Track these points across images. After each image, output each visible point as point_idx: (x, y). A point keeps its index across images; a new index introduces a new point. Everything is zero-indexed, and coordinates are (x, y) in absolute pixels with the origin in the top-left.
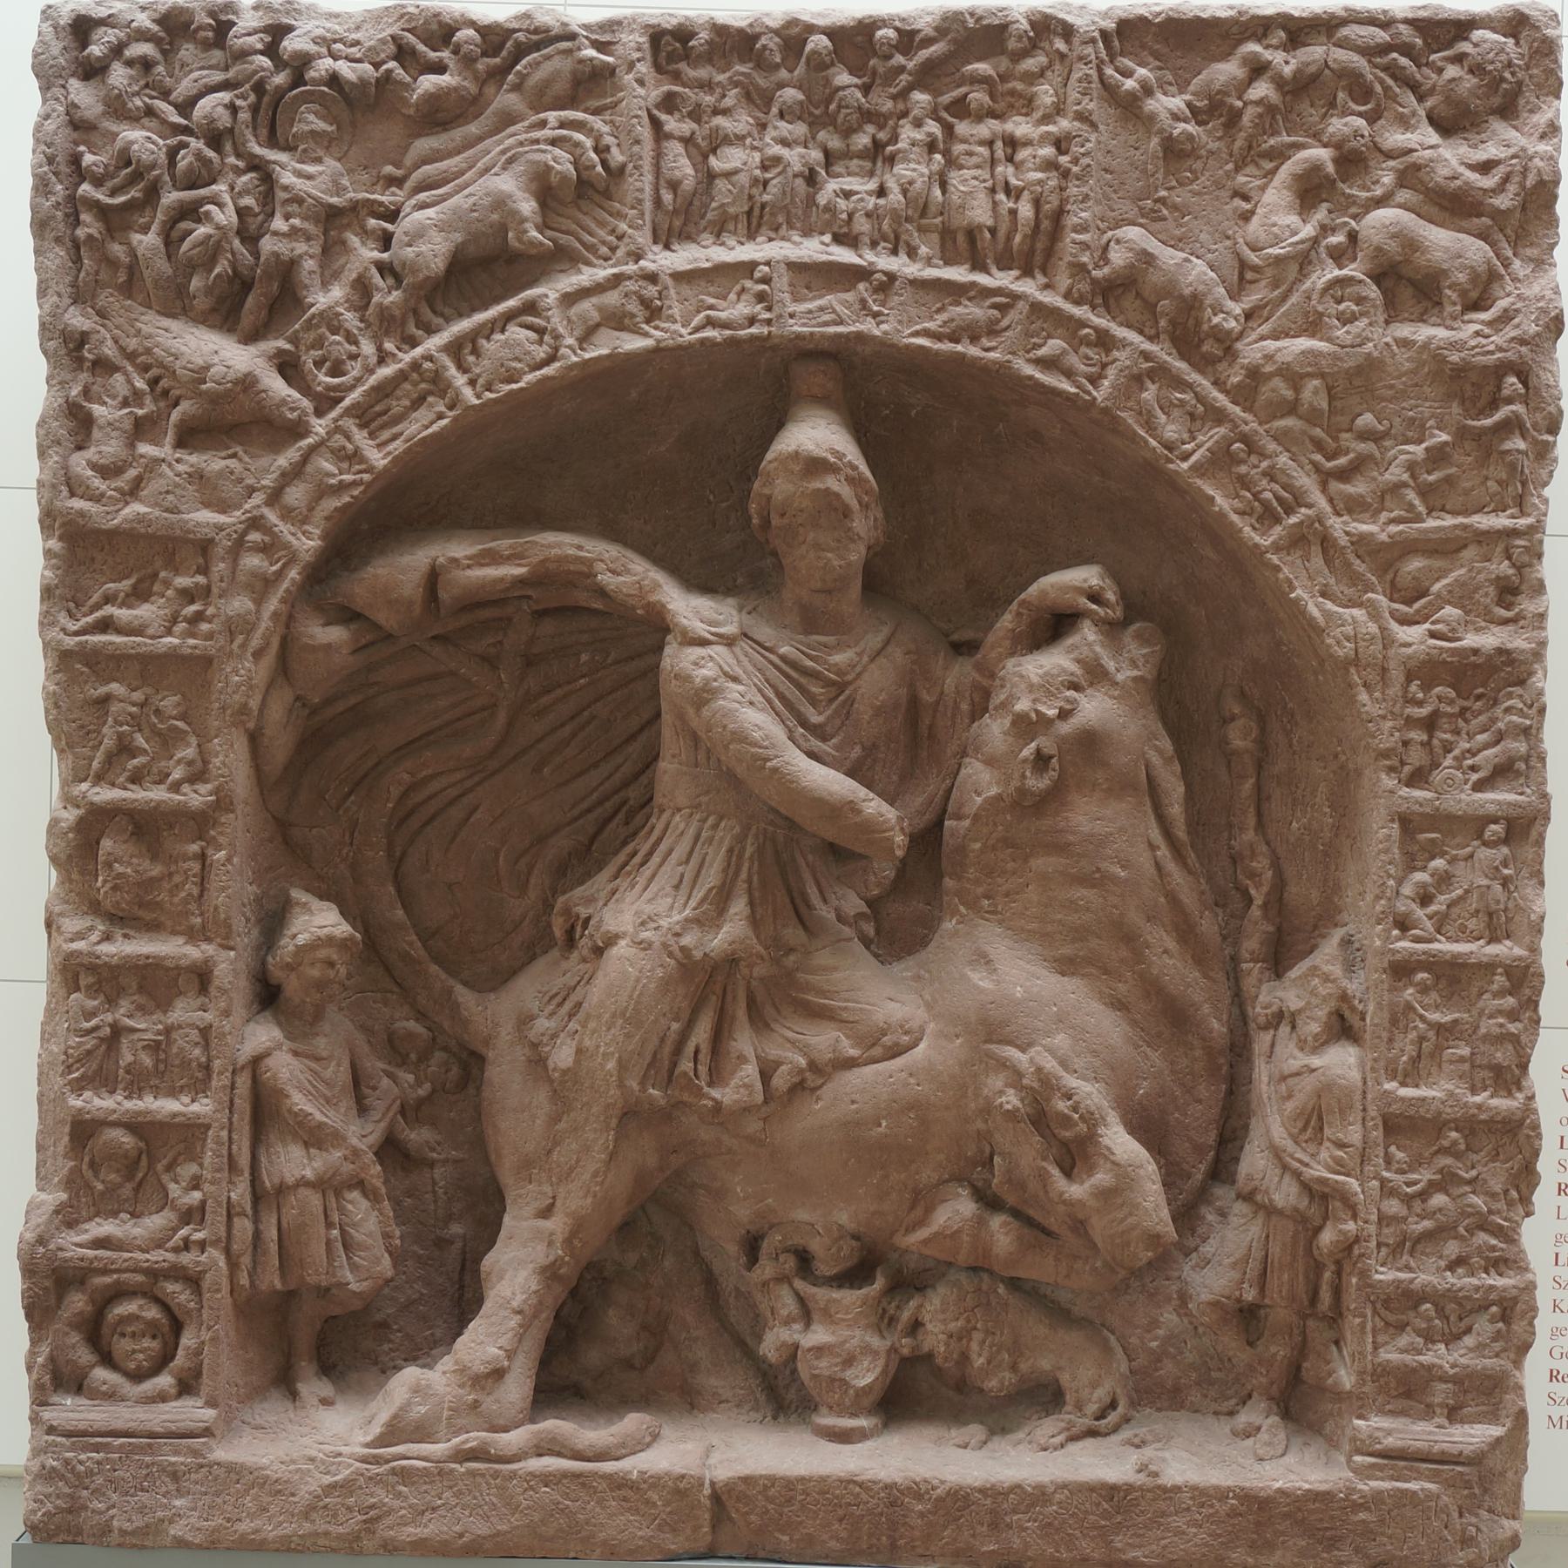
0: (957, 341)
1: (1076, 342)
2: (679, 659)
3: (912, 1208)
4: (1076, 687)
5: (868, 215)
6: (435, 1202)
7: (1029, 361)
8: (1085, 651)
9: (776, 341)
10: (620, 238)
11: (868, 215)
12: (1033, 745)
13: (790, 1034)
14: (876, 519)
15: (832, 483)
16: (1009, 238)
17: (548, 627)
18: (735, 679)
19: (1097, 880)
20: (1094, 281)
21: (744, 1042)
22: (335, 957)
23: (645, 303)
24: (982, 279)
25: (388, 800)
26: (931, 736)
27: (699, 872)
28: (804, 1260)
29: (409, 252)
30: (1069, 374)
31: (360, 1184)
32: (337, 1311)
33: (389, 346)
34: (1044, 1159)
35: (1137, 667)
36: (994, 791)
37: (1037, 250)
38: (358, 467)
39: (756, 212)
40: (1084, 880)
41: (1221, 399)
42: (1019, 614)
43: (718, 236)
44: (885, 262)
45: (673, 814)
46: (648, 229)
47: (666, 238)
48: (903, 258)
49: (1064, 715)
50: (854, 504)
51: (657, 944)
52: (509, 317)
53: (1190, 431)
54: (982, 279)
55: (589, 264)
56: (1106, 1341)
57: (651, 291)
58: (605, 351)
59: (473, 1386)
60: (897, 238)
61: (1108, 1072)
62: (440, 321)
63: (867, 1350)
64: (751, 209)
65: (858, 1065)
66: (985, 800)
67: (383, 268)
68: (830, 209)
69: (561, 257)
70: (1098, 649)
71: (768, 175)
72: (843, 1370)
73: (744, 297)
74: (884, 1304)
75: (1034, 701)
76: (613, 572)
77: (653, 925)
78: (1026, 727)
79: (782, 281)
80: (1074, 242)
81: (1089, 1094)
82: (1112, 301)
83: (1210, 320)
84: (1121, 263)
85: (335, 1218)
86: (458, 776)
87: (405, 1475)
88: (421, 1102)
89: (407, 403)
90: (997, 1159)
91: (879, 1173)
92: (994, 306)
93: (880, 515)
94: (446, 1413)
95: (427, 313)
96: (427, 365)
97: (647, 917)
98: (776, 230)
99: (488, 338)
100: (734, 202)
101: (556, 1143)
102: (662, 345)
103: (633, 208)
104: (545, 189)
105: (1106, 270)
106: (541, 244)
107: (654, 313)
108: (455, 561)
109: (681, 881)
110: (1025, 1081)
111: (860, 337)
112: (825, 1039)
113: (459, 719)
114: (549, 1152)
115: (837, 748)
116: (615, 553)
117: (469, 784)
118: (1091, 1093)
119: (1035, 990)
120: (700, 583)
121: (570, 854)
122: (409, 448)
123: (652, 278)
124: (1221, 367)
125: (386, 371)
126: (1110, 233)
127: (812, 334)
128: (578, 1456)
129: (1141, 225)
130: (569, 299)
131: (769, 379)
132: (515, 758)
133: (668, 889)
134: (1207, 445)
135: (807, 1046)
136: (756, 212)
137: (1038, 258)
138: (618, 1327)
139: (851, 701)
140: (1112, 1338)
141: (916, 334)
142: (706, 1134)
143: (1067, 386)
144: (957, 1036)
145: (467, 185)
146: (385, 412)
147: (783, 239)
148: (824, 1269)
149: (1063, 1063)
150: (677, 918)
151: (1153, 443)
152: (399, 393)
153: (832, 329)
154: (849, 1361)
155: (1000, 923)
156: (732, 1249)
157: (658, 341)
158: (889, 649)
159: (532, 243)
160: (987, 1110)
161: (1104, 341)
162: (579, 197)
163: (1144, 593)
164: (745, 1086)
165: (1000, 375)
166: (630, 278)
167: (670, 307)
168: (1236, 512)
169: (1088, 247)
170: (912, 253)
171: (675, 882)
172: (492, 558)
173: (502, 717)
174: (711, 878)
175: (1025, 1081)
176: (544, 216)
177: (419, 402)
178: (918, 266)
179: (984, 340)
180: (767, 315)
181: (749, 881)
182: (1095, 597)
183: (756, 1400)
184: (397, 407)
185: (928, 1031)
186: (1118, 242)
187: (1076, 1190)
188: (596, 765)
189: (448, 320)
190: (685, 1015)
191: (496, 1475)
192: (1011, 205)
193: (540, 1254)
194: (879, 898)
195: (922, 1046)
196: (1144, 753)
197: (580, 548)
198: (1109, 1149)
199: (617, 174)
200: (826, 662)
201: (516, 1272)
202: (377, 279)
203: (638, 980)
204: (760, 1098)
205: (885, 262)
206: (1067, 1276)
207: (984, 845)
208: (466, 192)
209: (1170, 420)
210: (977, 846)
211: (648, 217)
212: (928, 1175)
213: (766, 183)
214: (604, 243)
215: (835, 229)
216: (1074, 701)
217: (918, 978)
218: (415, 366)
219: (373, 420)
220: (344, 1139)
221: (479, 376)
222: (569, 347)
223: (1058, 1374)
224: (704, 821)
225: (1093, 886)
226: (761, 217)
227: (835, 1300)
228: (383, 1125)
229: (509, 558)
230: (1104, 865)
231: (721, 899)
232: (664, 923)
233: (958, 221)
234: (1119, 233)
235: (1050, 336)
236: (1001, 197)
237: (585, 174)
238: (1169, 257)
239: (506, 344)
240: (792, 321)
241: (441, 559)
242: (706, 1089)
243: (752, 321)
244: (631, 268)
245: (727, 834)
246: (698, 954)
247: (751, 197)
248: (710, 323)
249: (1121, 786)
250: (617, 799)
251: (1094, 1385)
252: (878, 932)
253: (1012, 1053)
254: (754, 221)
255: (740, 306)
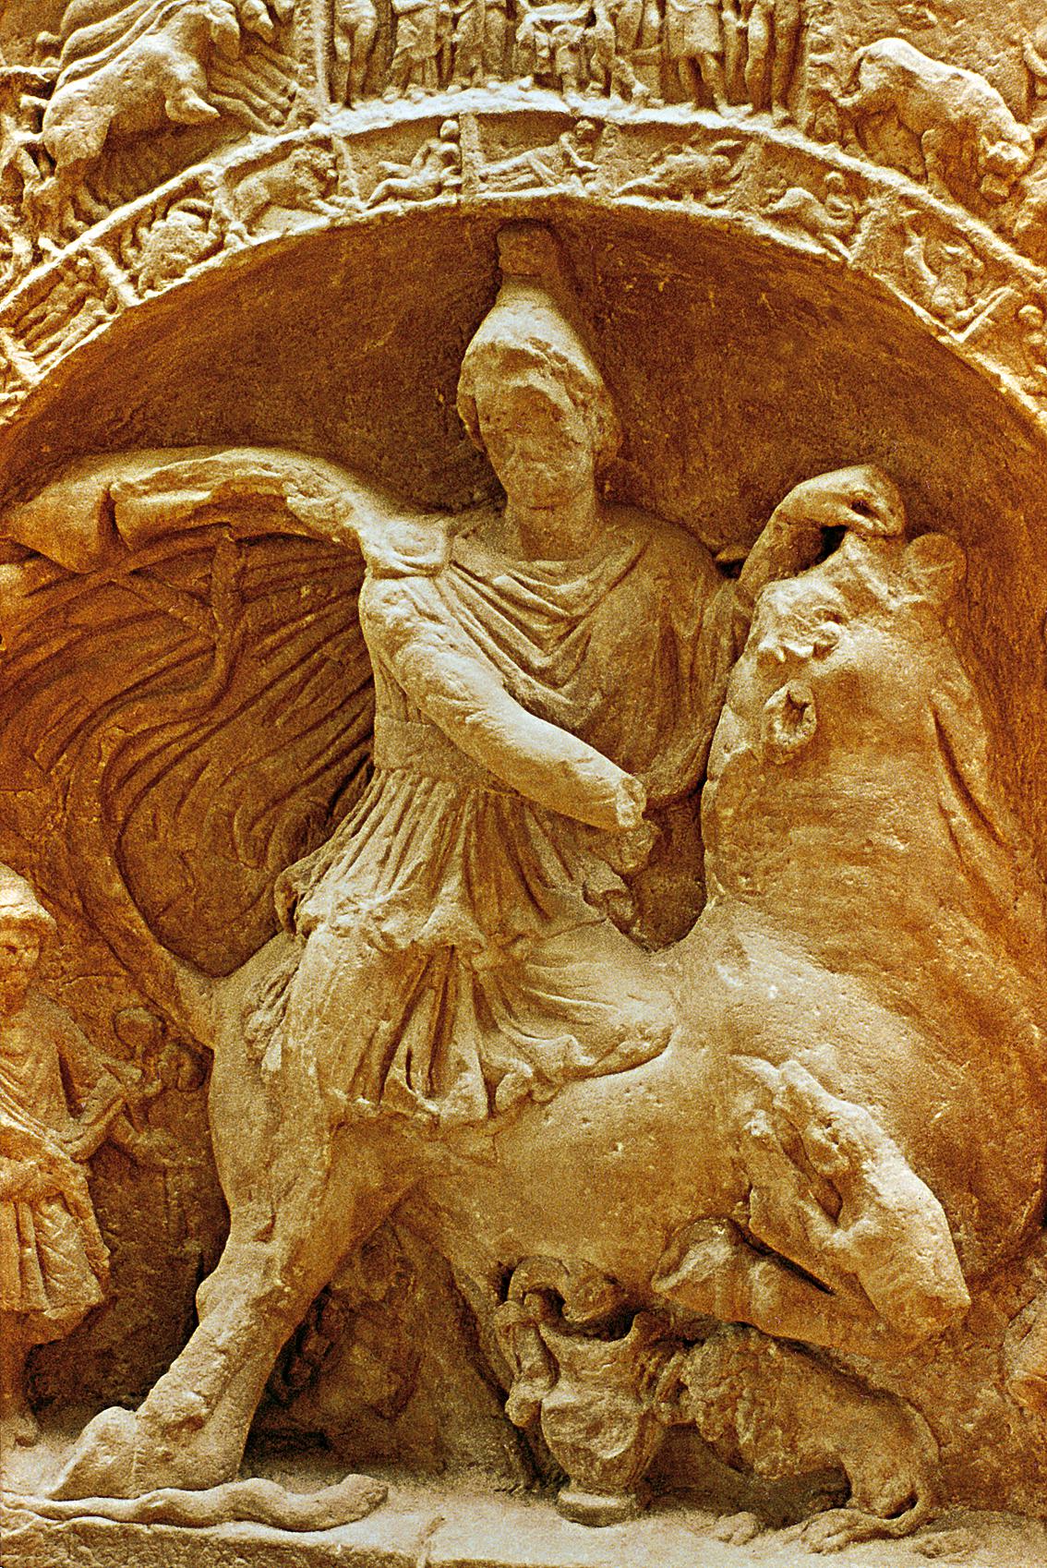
0: (678, 197)
1: (823, 191)
2: (373, 595)
3: (667, 1247)
4: (837, 619)
5: (573, 49)
6: (168, 1215)
7: (766, 217)
8: (847, 576)
9: (467, 210)
10: (292, 98)
11: (573, 49)
12: (783, 691)
13: (517, 1036)
14: (600, 420)
15: (534, 379)
16: (740, 66)
17: (259, 556)
18: (433, 618)
19: (865, 856)
20: (842, 111)
21: (466, 1045)
22: (15, 941)
23: (319, 174)
24: (708, 119)
25: (99, 758)
26: (693, 677)
27: (408, 844)
28: (553, 1302)
29: (58, 132)
30: (814, 230)
31: (60, 1196)
32: (40, 1340)
33: (45, 242)
34: (803, 1196)
35: (919, 591)
36: (744, 746)
37: (775, 76)
38: (12, 384)
39: (447, 54)
40: (855, 858)
41: (1005, 251)
42: (778, 528)
43: (405, 87)
44: (592, 105)
45: (388, 775)
46: (322, 86)
47: (344, 95)
48: (615, 97)
49: (821, 653)
50: (565, 403)
51: (355, 931)
52: (171, 200)
53: (968, 294)
54: (708, 119)
55: (259, 131)
56: (906, 1419)
57: (324, 159)
58: (275, 235)
59: (163, 1435)
60: (608, 75)
61: (889, 1092)
62: (102, 208)
63: (617, 1416)
64: (441, 52)
65: (593, 1076)
66: (734, 758)
67: (35, 151)
68: (530, 46)
69: (229, 125)
70: (864, 569)
71: (458, 10)
72: (587, 1439)
73: (430, 160)
74: (643, 1359)
75: (781, 637)
76: (305, 493)
77: (354, 907)
78: (779, 669)
79: (472, 136)
80: (813, 64)
81: (853, 1121)
82: (869, 134)
83: (985, 151)
84: (873, 86)
85: (30, 1234)
86: (181, 729)
87: (86, 1535)
88: (146, 1104)
89: (64, 307)
90: (753, 1194)
91: (620, 1206)
92: (721, 151)
93: (607, 413)
94: (135, 1465)
95: (87, 201)
96: (83, 262)
97: (354, 897)
98: (471, 73)
99: (149, 226)
100: (418, 46)
101: (274, 1156)
102: (338, 223)
103: (302, 61)
104: (205, 44)
105: (857, 97)
106: (202, 112)
107: (329, 187)
108: (128, 486)
109: (387, 855)
110: (777, 1103)
111: (564, 200)
112: (552, 1043)
113: (177, 664)
114: (268, 1165)
115: (573, 695)
116: (307, 472)
117: (195, 737)
118: (857, 1119)
119: (793, 990)
120: (409, 497)
121: (308, 818)
122: (67, 360)
123: (325, 144)
124: (1004, 210)
125: (39, 272)
126: (862, 50)
127: (506, 200)
128: (278, 1524)
129: (901, 36)
130: (236, 174)
131: (476, 254)
132: (243, 708)
133: (373, 865)
134: (988, 311)
135: (533, 1051)
136: (447, 54)
137: (776, 88)
138: (367, 1369)
139: (586, 638)
140: (918, 1416)
141: (630, 192)
142: (432, 1152)
143: (809, 246)
144: (703, 1045)
145: (124, 47)
146: (42, 318)
147: (478, 85)
148: (575, 1316)
149: (825, 1083)
150: (380, 898)
151: (920, 311)
152: (54, 296)
153: (528, 194)
154: (595, 1428)
155: (761, 904)
156: (482, 1283)
157: (333, 220)
158: (634, 574)
159: (191, 112)
160: (737, 1136)
161: (857, 186)
162: (249, 51)
163: (949, 494)
164: (465, 1098)
165: (730, 236)
166: (301, 145)
167: (345, 178)
168: (1028, 391)
169: (832, 69)
170: (626, 94)
171: (381, 856)
172: (167, 482)
173: (220, 665)
174: (419, 855)
175: (777, 1103)
176: (209, 80)
177: (77, 305)
178: (632, 107)
179: (709, 194)
180: (455, 180)
181: (465, 856)
182: (861, 507)
183: (509, 1464)
184: (53, 312)
185: (673, 1037)
186: (871, 59)
187: (840, 1238)
188: (331, 715)
189: (111, 207)
190: (398, 1014)
191: (186, 1540)
192: (741, 24)
193: (255, 1285)
194: (640, 872)
195: (667, 1053)
196: (930, 698)
197: (267, 467)
198: (874, 1189)
199: (284, 22)
200: (551, 593)
201: (228, 1304)
202: (28, 166)
203: (334, 973)
204: (482, 1112)
205: (592, 105)
206: (845, 1339)
207: (737, 812)
208: (119, 57)
209: (942, 281)
210: (730, 812)
211: (321, 72)
212: (678, 1211)
213: (456, 19)
214: (275, 105)
215: (536, 70)
216: (832, 637)
217: (671, 970)
218: (70, 263)
219: (30, 328)
220: (38, 1145)
221: (140, 271)
222: (236, 232)
223: (842, 1457)
224: (416, 784)
225: (864, 863)
226: (453, 60)
227: (580, 1353)
228: (99, 1127)
229: (189, 481)
230: (876, 837)
231: (434, 875)
232: (364, 906)
233: (678, 50)
234: (874, 48)
235: (790, 184)
236: (728, 14)
237: (250, 25)
238: (931, 72)
239: (166, 234)
240: (483, 186)
241: (115, 486)
242: (421, 1100)
243: (439, 188)
244: (300, 134)
245: (443, 795)
246: (403, 943)
247: (439, 38)
248: (392, 194)
249: (902, 741)
250: (355, 754)
251: (887, 1475)
252: (640, 911)
253: (762, 1066)
254: (446, 66)
255: (425, 171)
